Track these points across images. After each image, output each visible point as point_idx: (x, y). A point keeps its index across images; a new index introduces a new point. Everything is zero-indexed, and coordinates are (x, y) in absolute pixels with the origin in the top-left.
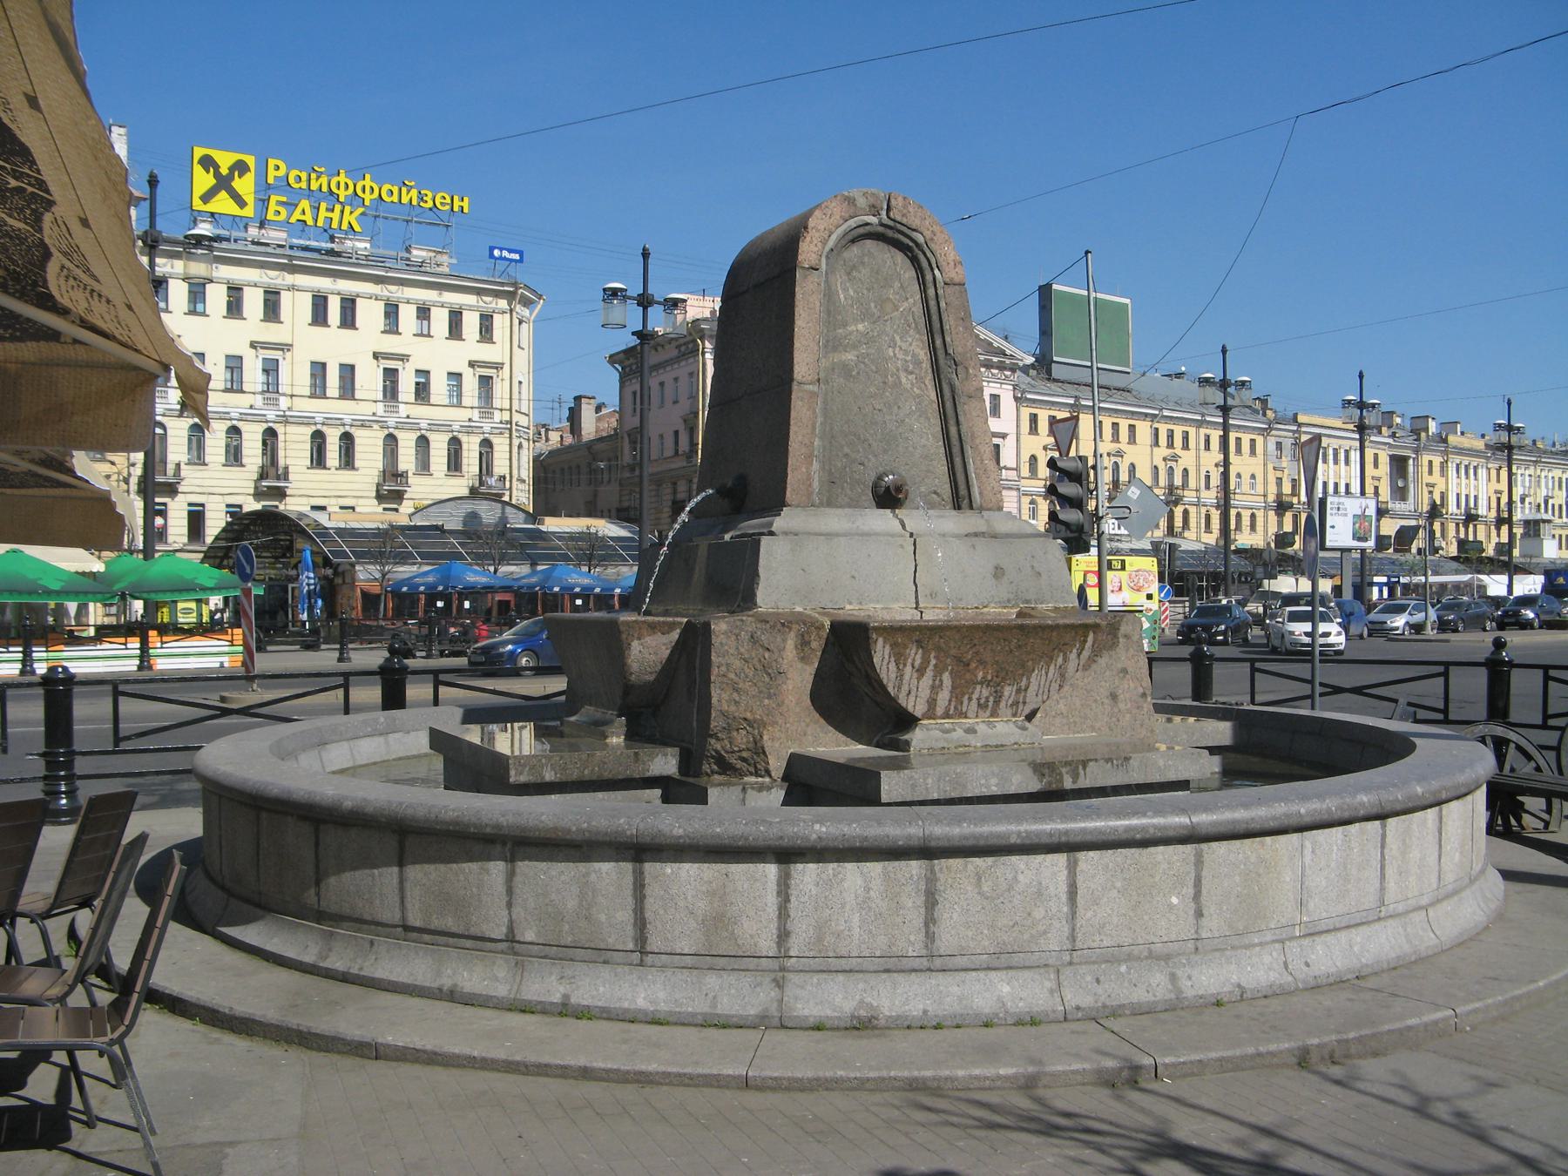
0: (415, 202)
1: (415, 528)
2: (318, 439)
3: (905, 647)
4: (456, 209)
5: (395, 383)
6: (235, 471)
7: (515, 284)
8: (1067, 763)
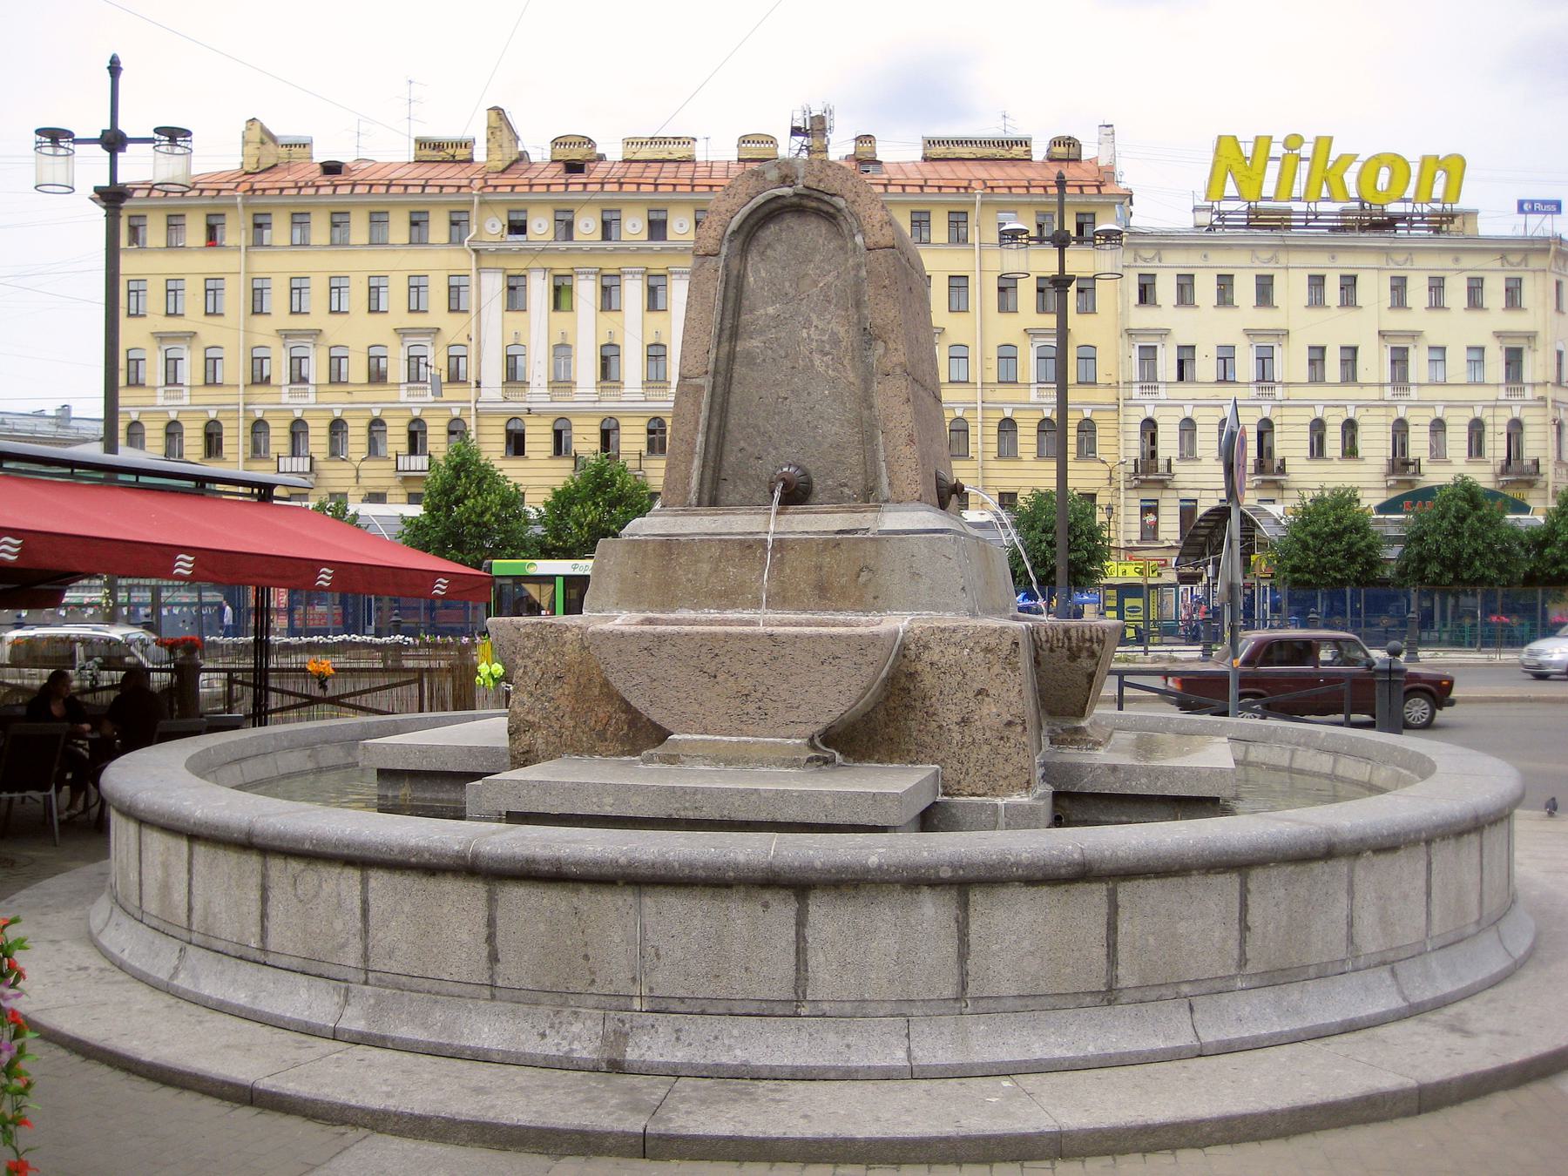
2: (1318, 427)
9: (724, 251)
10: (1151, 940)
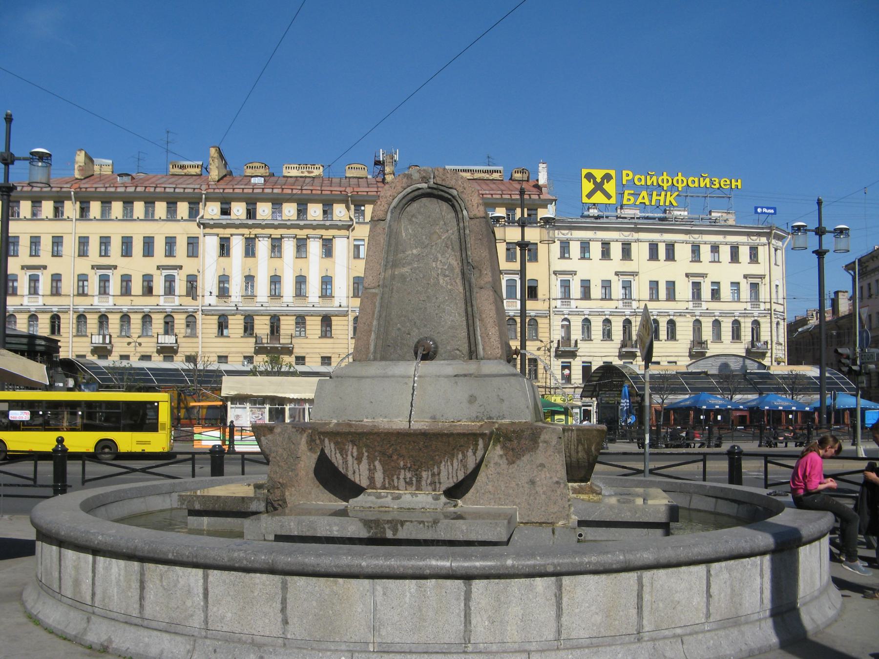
0: (708, 186)
1: (691, 373)
3: (344, 445)
4: (733, 187)
5: (699, 290)
6: (608, 344)
7: (770, 228)
8: (388, 522)
9: (389, 217)
10: (661, 605)
